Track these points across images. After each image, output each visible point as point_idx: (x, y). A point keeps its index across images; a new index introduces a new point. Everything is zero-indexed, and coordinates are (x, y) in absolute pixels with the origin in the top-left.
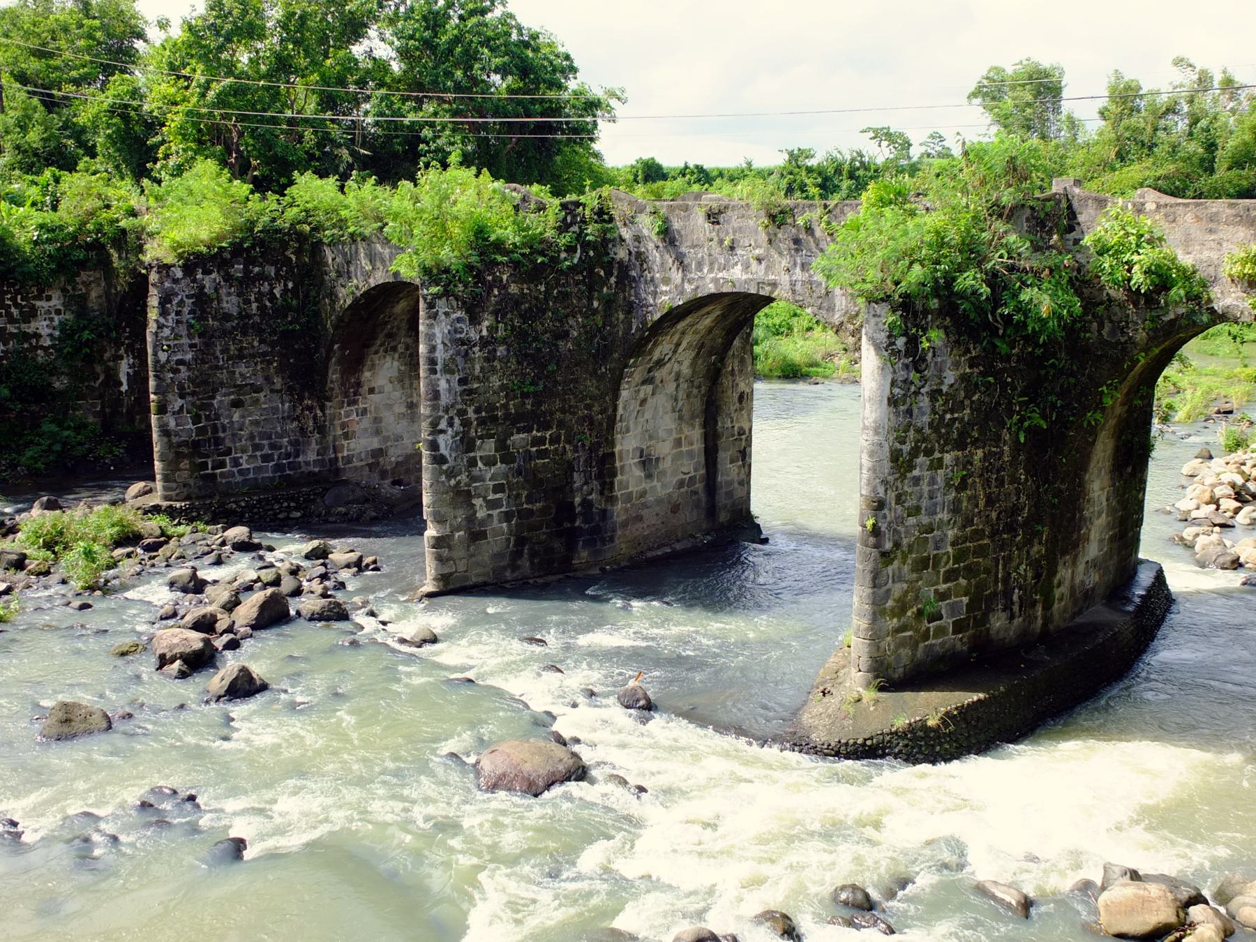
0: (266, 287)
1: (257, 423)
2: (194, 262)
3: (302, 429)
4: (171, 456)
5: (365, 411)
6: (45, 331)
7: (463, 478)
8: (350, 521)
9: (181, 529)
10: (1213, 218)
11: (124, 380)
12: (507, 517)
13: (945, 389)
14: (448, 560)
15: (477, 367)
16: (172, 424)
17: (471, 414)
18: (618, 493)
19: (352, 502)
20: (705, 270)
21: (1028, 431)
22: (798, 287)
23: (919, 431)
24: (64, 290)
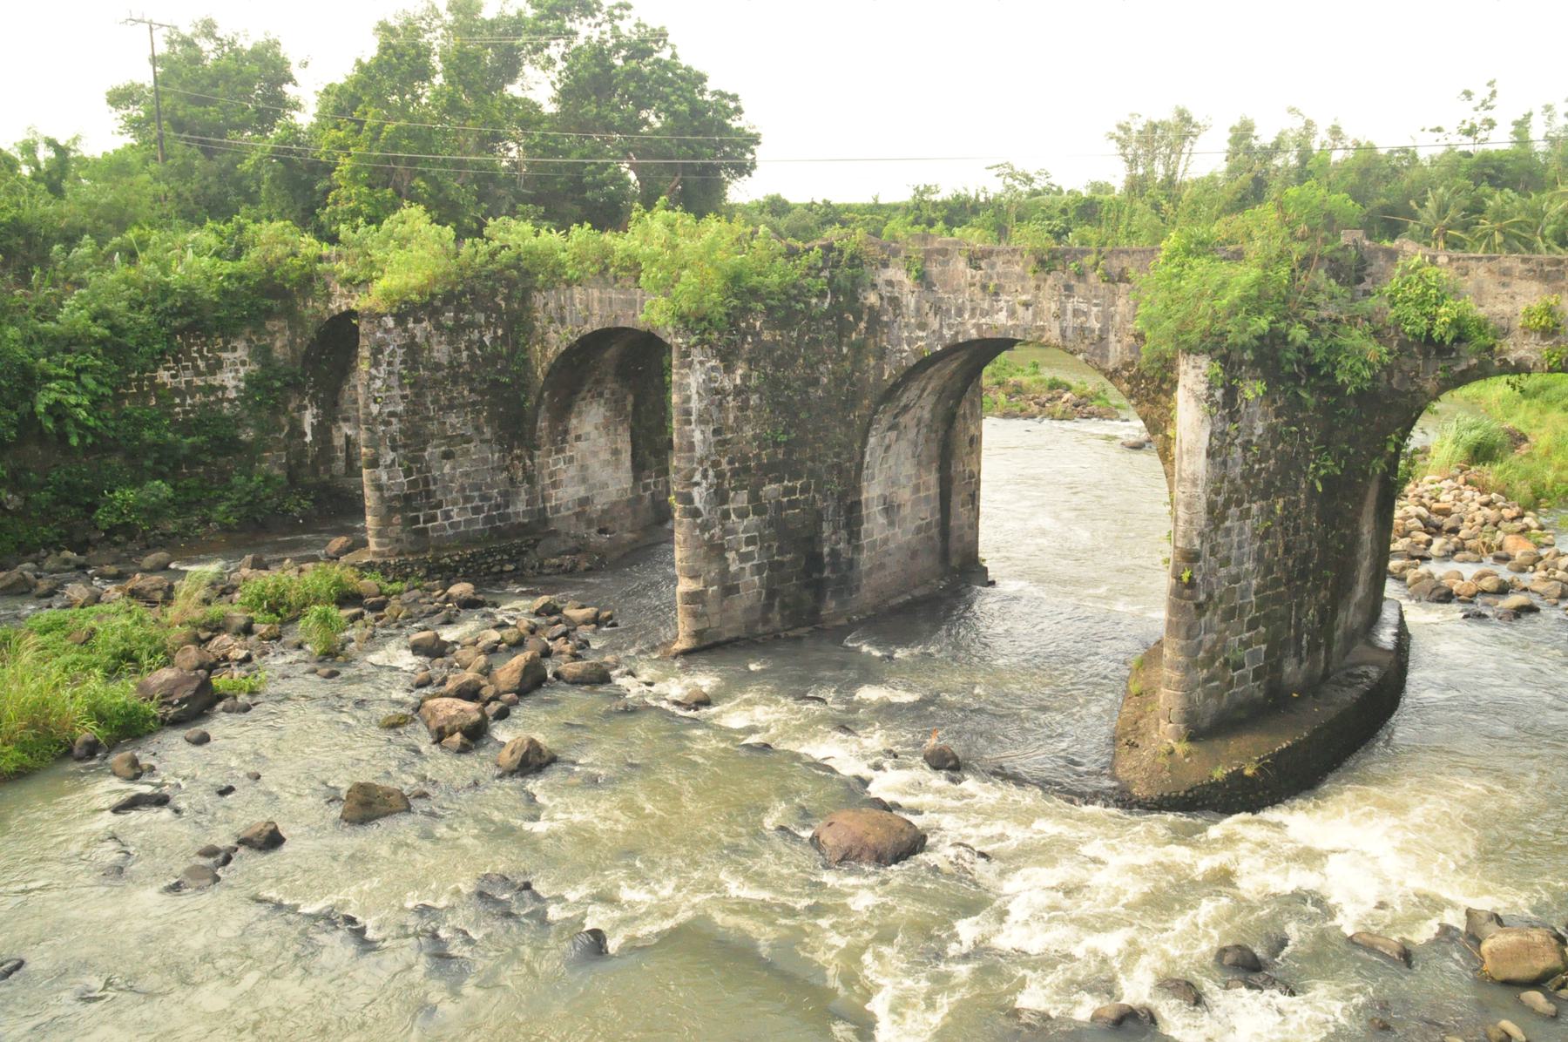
0: (476, 335)
1: (466, 474)
2: (405, 311)
3: (511, 479)
4: (384, 511)
5: (571, 460)
6: (230, 383)
7: (717, 531)
8: (565, 572)
9: (396, 586)
10: (1506, 272)
11: (308, 430)
12: (758, 569)
13: (1255, 439)
14: (702, 615)
15: (731, 417)
16: (384, 477)
17: (725, 466)
18: (864, 542)
19: (565, 553)
20: (966, 316)
21: (1322, 479)
22: (1069, 333)
23: (1232, 482)
24: (249, 341)
